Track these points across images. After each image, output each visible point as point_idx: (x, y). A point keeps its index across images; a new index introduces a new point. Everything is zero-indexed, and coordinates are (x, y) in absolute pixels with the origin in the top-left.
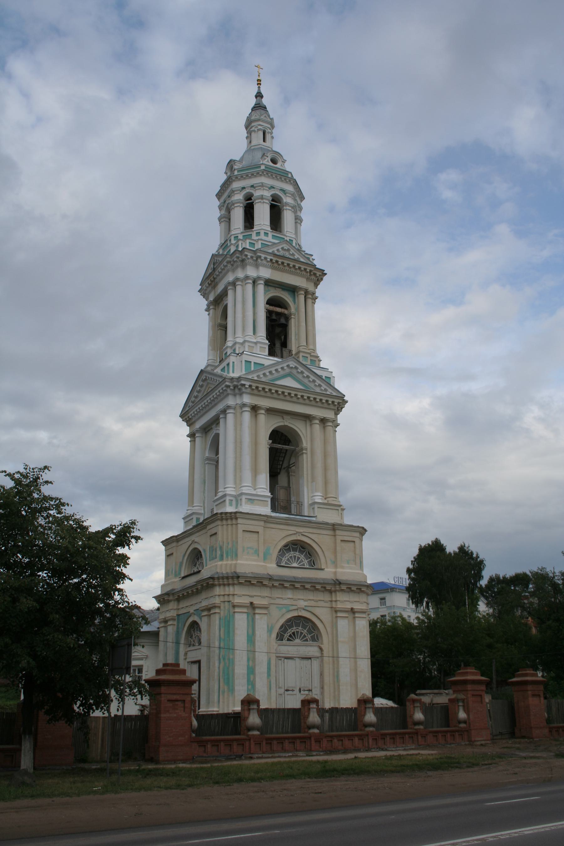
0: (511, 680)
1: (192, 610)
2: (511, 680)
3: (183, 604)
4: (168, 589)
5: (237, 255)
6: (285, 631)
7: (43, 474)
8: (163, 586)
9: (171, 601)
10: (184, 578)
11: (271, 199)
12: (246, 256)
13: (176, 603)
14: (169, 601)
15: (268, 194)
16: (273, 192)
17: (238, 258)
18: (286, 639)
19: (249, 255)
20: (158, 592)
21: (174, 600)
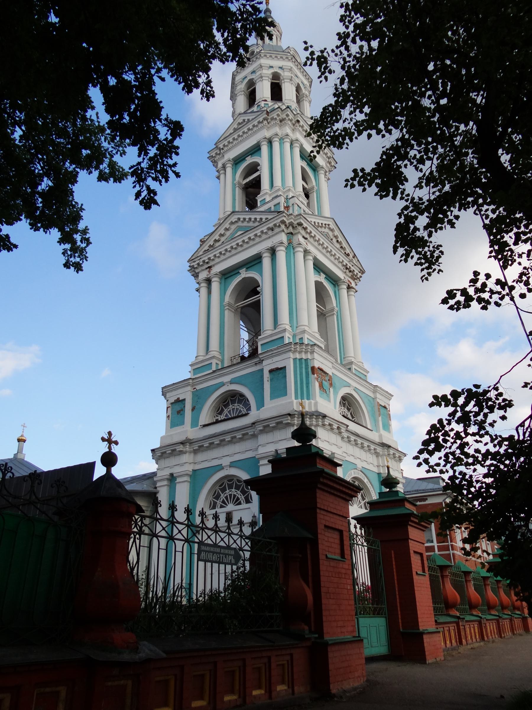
0: (308, 547)
1: (226, 462)
2: (308, 547)
3: (200, 457)
4: (169, 442)
5: (279, 112)
6: (217, 497)
7: (433, 244)
8: (162, 438)
9: (185, 453)
10: (205, 426)
11: (271, 77)
12: (287, 115)
13: (192, 454)
14: (181, 452)
15: (268, 72)
16: (271, 71)
17: (278, 115)
18: (219, 507)
19: (291, 117)
20: (157, 445)
21: (190, 452)
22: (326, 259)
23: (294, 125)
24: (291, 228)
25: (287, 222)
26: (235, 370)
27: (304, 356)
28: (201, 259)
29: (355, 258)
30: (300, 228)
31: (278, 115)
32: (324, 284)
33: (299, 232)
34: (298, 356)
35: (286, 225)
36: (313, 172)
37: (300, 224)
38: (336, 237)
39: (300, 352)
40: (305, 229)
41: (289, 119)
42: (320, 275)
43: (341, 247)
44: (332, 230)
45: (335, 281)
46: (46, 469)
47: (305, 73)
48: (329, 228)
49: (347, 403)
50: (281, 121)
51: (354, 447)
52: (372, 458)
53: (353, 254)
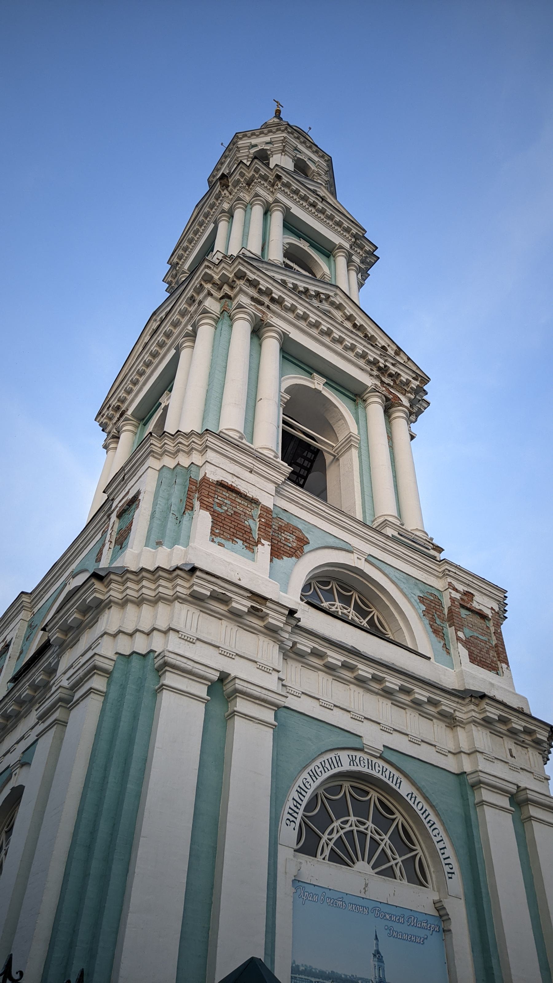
22: (323, 349)
23: (273, 186)
24: (226, 287)
25: (216, 277)
26: (82, 545)
27: (185, 461)
28: (110, 406)
29: (402, 355)
30: (241, 283)
31: (242, 175)
32: (324, 392)
33: (241, 290)
34: (170, 462)
35: (214, 284)
36: (326, 258)
37: (240, 276)
38: (350, 318)
39: (175, 454)
40: (254, 284)
41: (260, 175)
42: (313, 378)
43: (355, 326)
44: (339, 307)
45: (356, 395)
46: (275, 975)
47: (315, 149)
48: (332, 304)
49: (355, 596)
50: (249, 184)
51: (381, 699)
52: (435, 731)
53: (395, 348)
